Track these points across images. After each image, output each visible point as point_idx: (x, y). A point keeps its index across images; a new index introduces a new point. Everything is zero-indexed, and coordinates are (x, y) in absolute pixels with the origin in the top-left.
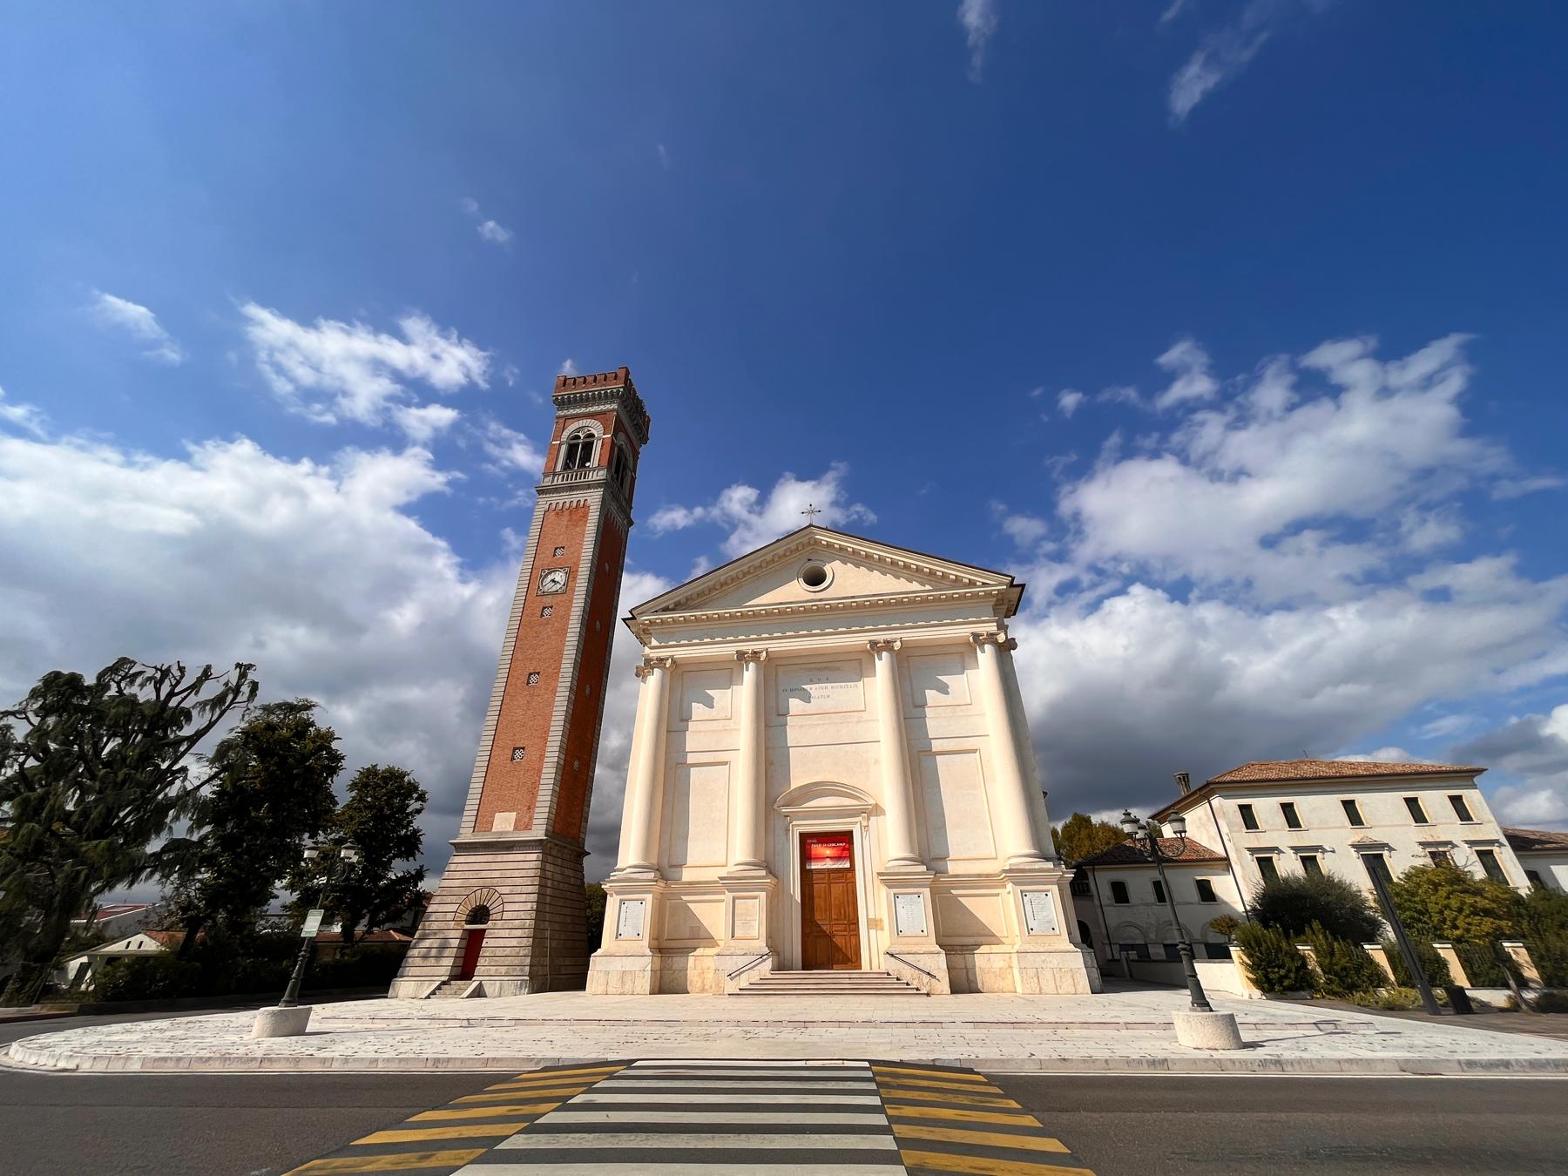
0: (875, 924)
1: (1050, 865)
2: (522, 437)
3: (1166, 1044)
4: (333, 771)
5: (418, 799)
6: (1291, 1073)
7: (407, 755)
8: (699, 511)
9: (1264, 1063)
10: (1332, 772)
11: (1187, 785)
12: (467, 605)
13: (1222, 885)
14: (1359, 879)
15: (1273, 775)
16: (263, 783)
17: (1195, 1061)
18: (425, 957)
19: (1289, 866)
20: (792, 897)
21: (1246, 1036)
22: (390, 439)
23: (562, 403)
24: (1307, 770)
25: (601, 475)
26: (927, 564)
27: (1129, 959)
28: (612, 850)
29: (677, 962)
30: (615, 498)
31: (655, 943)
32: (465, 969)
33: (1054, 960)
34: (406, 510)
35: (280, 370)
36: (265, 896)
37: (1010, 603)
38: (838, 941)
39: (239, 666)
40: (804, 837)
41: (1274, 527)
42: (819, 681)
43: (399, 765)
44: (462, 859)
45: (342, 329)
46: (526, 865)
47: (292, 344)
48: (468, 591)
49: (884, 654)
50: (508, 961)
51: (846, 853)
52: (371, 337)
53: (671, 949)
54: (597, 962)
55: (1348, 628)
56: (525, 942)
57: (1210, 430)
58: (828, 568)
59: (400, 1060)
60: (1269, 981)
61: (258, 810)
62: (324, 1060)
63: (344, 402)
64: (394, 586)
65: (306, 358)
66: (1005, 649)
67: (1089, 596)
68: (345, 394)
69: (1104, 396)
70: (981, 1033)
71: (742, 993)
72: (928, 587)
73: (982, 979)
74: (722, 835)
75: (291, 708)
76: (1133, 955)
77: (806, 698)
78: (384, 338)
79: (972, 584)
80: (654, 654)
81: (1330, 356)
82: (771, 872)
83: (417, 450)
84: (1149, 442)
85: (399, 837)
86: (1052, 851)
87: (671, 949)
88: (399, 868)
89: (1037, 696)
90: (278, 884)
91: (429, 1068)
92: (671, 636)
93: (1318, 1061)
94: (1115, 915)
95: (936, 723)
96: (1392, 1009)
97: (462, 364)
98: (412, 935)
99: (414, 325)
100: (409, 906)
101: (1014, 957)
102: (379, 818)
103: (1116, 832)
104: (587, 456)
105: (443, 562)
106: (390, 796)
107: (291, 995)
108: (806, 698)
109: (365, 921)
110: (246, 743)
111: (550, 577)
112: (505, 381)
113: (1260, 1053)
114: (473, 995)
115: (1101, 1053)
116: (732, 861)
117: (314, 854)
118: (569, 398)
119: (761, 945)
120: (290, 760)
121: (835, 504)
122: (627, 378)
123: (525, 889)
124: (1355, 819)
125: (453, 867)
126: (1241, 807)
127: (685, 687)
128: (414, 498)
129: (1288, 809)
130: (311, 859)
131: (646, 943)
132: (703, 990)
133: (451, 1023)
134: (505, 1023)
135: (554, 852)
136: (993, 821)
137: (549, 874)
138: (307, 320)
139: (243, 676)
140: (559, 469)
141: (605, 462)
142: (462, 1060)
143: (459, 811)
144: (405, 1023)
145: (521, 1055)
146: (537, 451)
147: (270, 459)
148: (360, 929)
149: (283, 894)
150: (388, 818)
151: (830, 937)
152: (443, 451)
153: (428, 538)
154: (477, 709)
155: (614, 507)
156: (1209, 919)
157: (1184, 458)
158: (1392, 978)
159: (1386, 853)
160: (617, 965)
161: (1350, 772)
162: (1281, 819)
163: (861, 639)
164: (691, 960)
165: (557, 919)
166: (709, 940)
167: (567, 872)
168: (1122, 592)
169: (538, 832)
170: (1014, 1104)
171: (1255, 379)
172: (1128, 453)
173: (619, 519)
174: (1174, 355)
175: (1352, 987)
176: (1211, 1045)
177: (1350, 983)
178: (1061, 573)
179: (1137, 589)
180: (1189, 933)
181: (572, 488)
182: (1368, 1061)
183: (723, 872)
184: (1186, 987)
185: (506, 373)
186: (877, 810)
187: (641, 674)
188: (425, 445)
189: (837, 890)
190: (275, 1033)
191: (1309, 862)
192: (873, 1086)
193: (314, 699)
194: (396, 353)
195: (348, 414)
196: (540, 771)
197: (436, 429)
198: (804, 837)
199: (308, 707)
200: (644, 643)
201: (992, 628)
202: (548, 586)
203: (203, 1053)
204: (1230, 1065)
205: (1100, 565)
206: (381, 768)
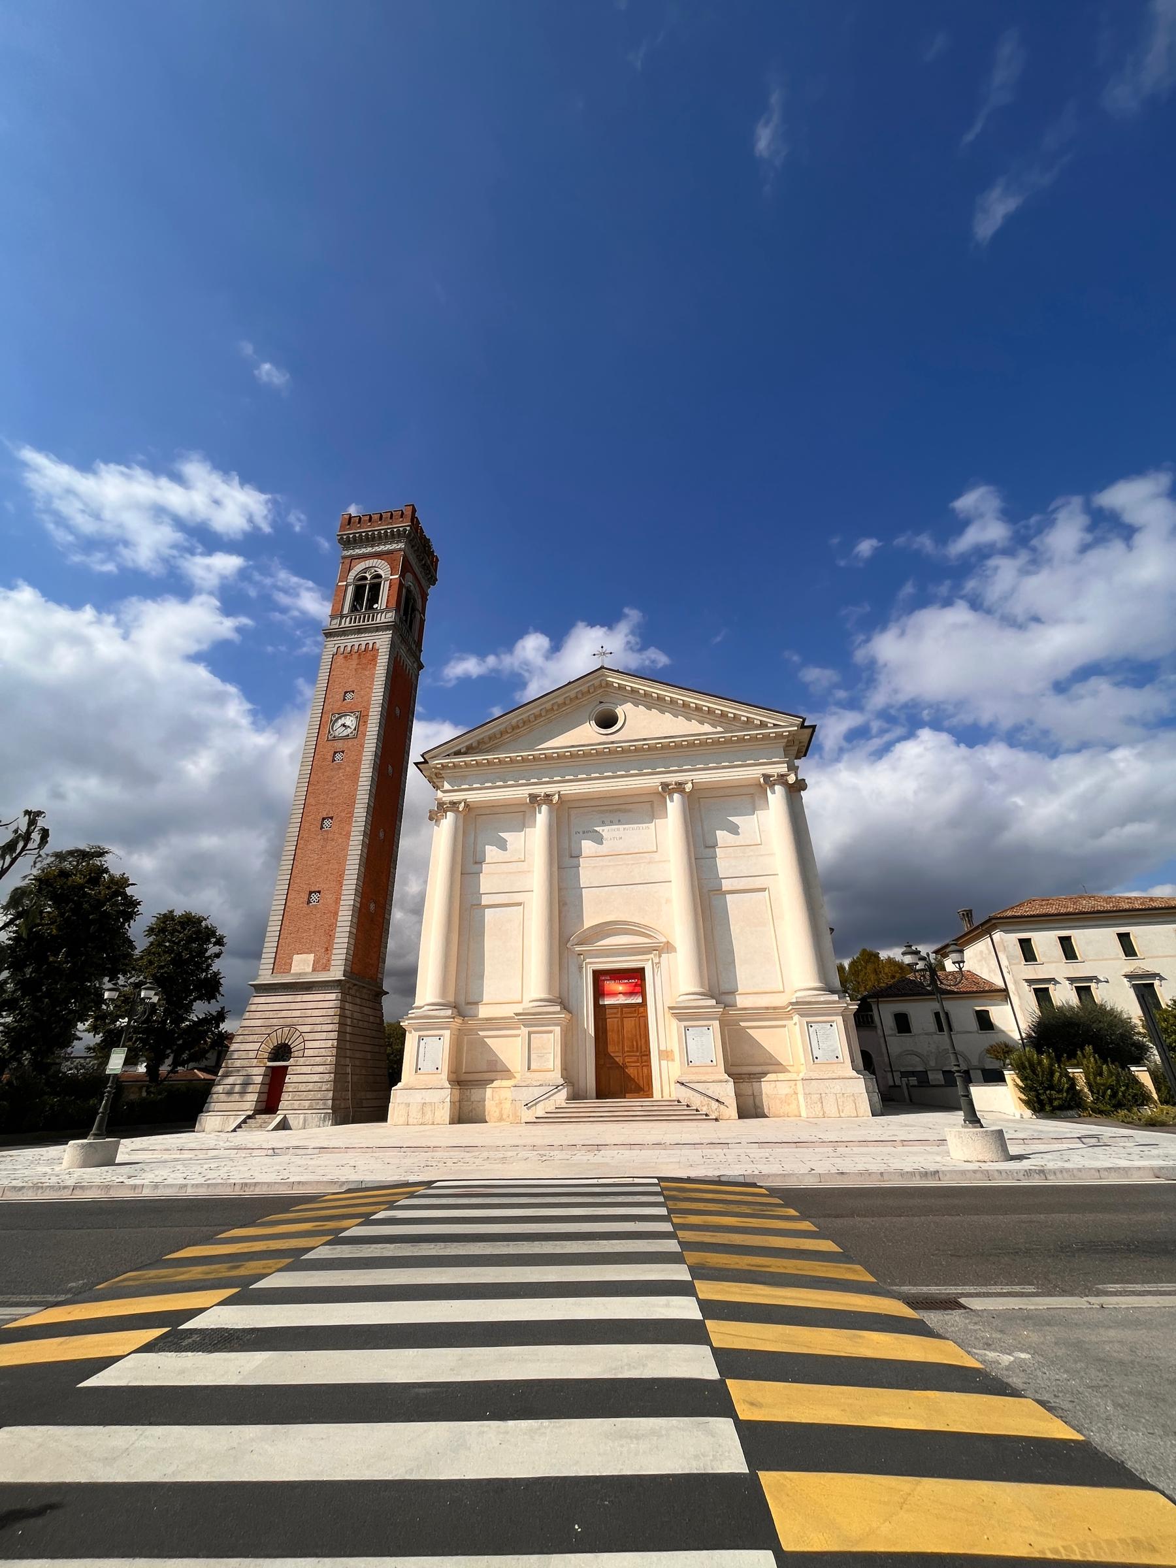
0: (666, 1055)
1: (835, 997)
2: (310, 584)
3: (938, 1159)
4: (129, 916)
5: (215, 944)
6: (1052, 1181)
7: (211, 904)
8: (491, 660)
9: (1028, 1173)
10: (1109, 907)
11: (970, 921)
12: (264, 756)
13: (1000, 1015)
14: (1130, 1008)
15: (1053, 911)
16: (59, 929)
17: (963, 1172)
18: (229, 1093)
19: (1064, 996)
20: (585, 1031)
21: (1013, 1150)
22: (173, 585)
23: (347, 543)
24: (1086, 905)
25: (390, 617)
26: (719, 706)
27: (903, 1086)
28: (410, 991)
29: (475, 1094)
30: (404, 640)
31: (454, 1077)
32: (269, 1103)
33: (837, 1086)
34: (195, 658)
35: (62, 521)
36: (68, 1038)
37: (801, 746)
38: (631, 1071)
39: (27, 813)
40: (598, 975)
41: (1063, 672)
42: (612, 823)
43: (196, 910)
44: (262, 1000)
45: (122, 474)
46: (326, 1005)
47: (70, 492)
48: (262, 740)
49: (676, 796)
50: (311, 1095)
51: (638, 989)
52: (151, 482)
53: (469, 1083)
54: (398, 1095)
55: (1130, 771)
56: (326, 1077)
57: (1004, 574)
58: (619, 711)
59: (209, 1185)
60: (1040, 1102)
61: (56, 955)
62: (135, 1187)
63: (125, 552)
64: (188, 734)
65: (86, 504)
66: (795, 790)
67: (876, 743)
68: (126, 543)
69: (900, 541)
70: (766, 1152)
71: (539, 1121)
72: (720, 729)
73: (768, 1104)
74: (518, 970)
75: (83, 855)
76: (913, 1080)
77: (599, 839)
78: (164, 482)
79: (763, 725)
80: (447, 798)
81: (1132, 497)
82: (565, 1007)
83: (204, 598)
84: (944, 589)
85: (199, 980)
86: (837, 983)
87: (469, 1083)
88: (200, 1010)
89: (827, 841)
90: (80, 1026)
91: (237, 1192)
92: (463, 779)
93: (1079, 1170)
94: (897, 1044)
95: (727, 864)
96: (1153, 1125)
97: (244, 507)
98: (216, 1074)
99: (195, 469)
100: (211, 1046)
101: (800, 1084)
102: (178, 962)
103: (900, 966)
104: (374, 598)
105: (236, 709)
106: (188, 939)
107: (99, 1128)
108: (599, 839)
109: (169, 1061)
110: (40, 890)
111: (340, 722)
112: (290, 526)
113: (1025, 1164)
114: (278, 1128)
115: (874, 1167)
116: (527, 998)
117: (115, 995)
118: (353, 538)
119: (556, 1077)
120: (85, 906)
121: (629, 647)
122: (413, 518)
123: (325, 1028)
124: (1129, 949)
125: (253, 1008)
126: (1021, 941)
127: (477, 828)
128: (204, 647)
129: (1065, 942)
130: (112, 1000)
131: (444, 1076)
132: (501, 1119)
133: (256, 1153)
134: (309, 1151)
135: (352, 992)
136: (781, 957)
137: (348, 1013)
138: (85, 465)
139: (32, 822)
140: (346, 611)
141: (393, 604)
142: (269, 1184)
143: (258, 955)
144: (212, 1153)
145: (325, 1179)
146: (325, 598)
147: (52, 606)
148: (164, 1069)
149: (86, 1036)
150: (188, 962)
151: (622, 1068)
152: (231, 599)
153: (217, 684)
154: (275, 855)
155: (403, 651)
156: (987, 1046)
157: (975, 604)
158: (1155, 1096)
159: (1156, 983)
160: (417, 1097)
161: (1127, 906)
162: (1058, 951)
163: (653, 782)
164: (489, 1092)
165: (358, 1055)
166: (506, 1073)
167: (366, 1011)
168: (910, 735)
169: (336, 972)
170: (792, 1212)
171: (1049, 523)
172: (922, 601)
173: (409, 662)
174: (967, 502)
175: (1119, 1105)
176: (980, 1158)
177: (1118, 1103)
178: (851, 720)
179: (925, 734)
180: (966, 1059)
181: (359, 631)
182: (1126, 1170)
183: (519, 1009)
184: (960, 1109)
185: (292, 518)
186: (668, 948)
187: (435, 816)
188: (211, 593)
189: (629, 1024)
190: (85, 1164)
191: (1084, 992)
192: (661, 1199)
193: (107, 847)
194: (174, 497)
195: (130, 565)
196: (336, 914)
197: (223, 577)
198: (598, 975)
199: (101, 854)
200: (436, 787)
201: (783, 769)
202: (339, 731)
203: (14, 1183)
204: (996, 1174)
205: (893, 712)
206: (178, 913)
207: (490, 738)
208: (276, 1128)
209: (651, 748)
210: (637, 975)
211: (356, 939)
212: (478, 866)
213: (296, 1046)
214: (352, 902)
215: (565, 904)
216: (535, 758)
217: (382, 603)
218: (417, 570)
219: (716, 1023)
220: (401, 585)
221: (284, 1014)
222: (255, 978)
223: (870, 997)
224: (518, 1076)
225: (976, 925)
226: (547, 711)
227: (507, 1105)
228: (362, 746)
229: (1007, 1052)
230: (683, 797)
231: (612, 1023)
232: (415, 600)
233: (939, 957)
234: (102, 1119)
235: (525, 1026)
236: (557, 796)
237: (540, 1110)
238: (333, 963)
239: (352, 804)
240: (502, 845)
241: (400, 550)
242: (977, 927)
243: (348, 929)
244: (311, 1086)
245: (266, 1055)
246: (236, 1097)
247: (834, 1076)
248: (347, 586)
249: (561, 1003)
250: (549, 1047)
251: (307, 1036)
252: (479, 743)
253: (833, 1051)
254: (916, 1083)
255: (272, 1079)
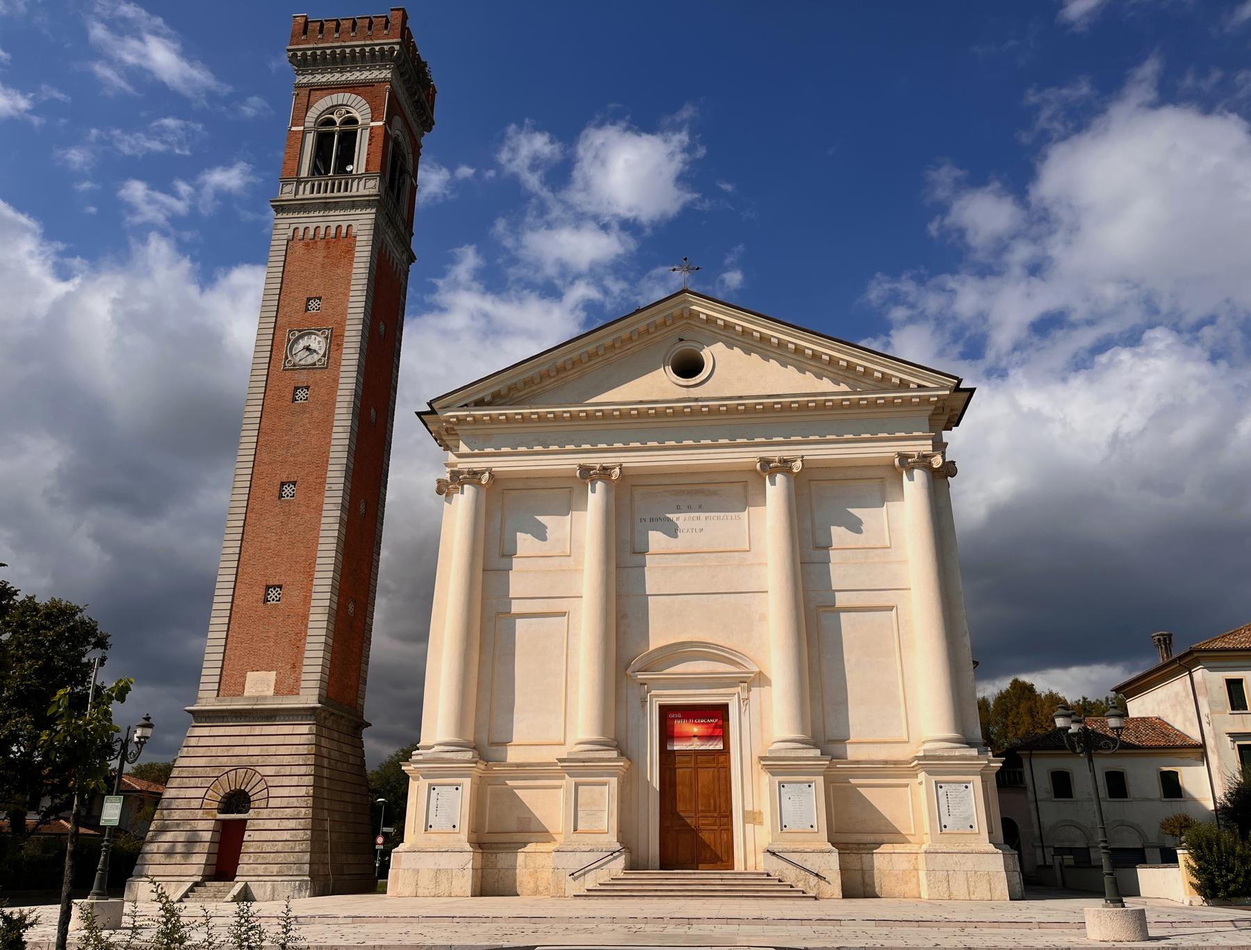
0: (752, 817)
1: (974, 752)
5: (96, 645)
11: (1168, 650)
18: (170, 853)
20: (649, 784)
21: (1152, 933)
23: (304, 63)
29: (503, 859)
30: (391, 222)
32: (223, 866)
33: (970, 862)
38: (706, 836)
42: (690, 509)
44: (205, 731)
46: (296, 740)
50: (280, 858)
51: (718, 732)
53: (496, 846)
58: (706, 354)
71: (590, 894)
74: (561, 704)
77: (672, 531)
79: (904, 385)
80: (464, 465)
86: (977, 733)
87: (496, 846)
92: (487, 439)
94: (1052, 812)
101: (922, 858)
104: (347, 155)
107: (100, 887)
108: (672, 531)
111: (303, 343)
123: (296, 770)
125: (193, 742)
127: (505, 512)
131: (464, 836)
132: (536, 892)
135: (329, 723)
136: (908, 695)
137: (325, 751)
140: (304, 172)
141: (376, 167)
151: (694, 832)
155: (389, 238)
160: (428, 863)
164: (521, 857)
166: (543, 834)
167: (346, 749)
169: (309, 697)
173: (397, 254)
176: (1117, 937)
181: (327, 206)
183: (563, 753)
186: (760, 680)
189: (705, 776)
201: (926, 447)
207: (525, 383)
208: (236, 899)
209: (749, 410)
210: (719, 713)
211: (333, 653)
212: (505, 560)
213: (256, 793)
214: (327, 603)
215: (625, 616)
216: (589, 416)
217: (359, 164)
218: (408, 110)
219: (820, 779)
220: (387, 136)
221: (237, 751)
222: (195, 700)
223: (1022, 748)
224: (560, 839)
225: (1175, 656)
226: (606, 349)
227: (546, 875)
228: (336, 381)
229: (1186, 827)
230: (788, 481)
231: (682, 773)
232: (404, 158)
233: (1121, 696)
234: (102, 879)
235: (571, 775)
236: (617, 470)
237: (590, 881)
238: (303, 684)
239: (323, 465)
240: (540, 533)
241: (384, 81)
242: (1174, 661)
243: (323, 639)
244: (279, 846)
245: (215, 805)
246: (178, 858)
247: (967, 849)
248: (304, 133)
249: (617, 747)
250: (602, 804)
251: (271, 781)
252: (510, 389)
253: (967, 818)
254: (1072, 863)
255: (222, 835)
